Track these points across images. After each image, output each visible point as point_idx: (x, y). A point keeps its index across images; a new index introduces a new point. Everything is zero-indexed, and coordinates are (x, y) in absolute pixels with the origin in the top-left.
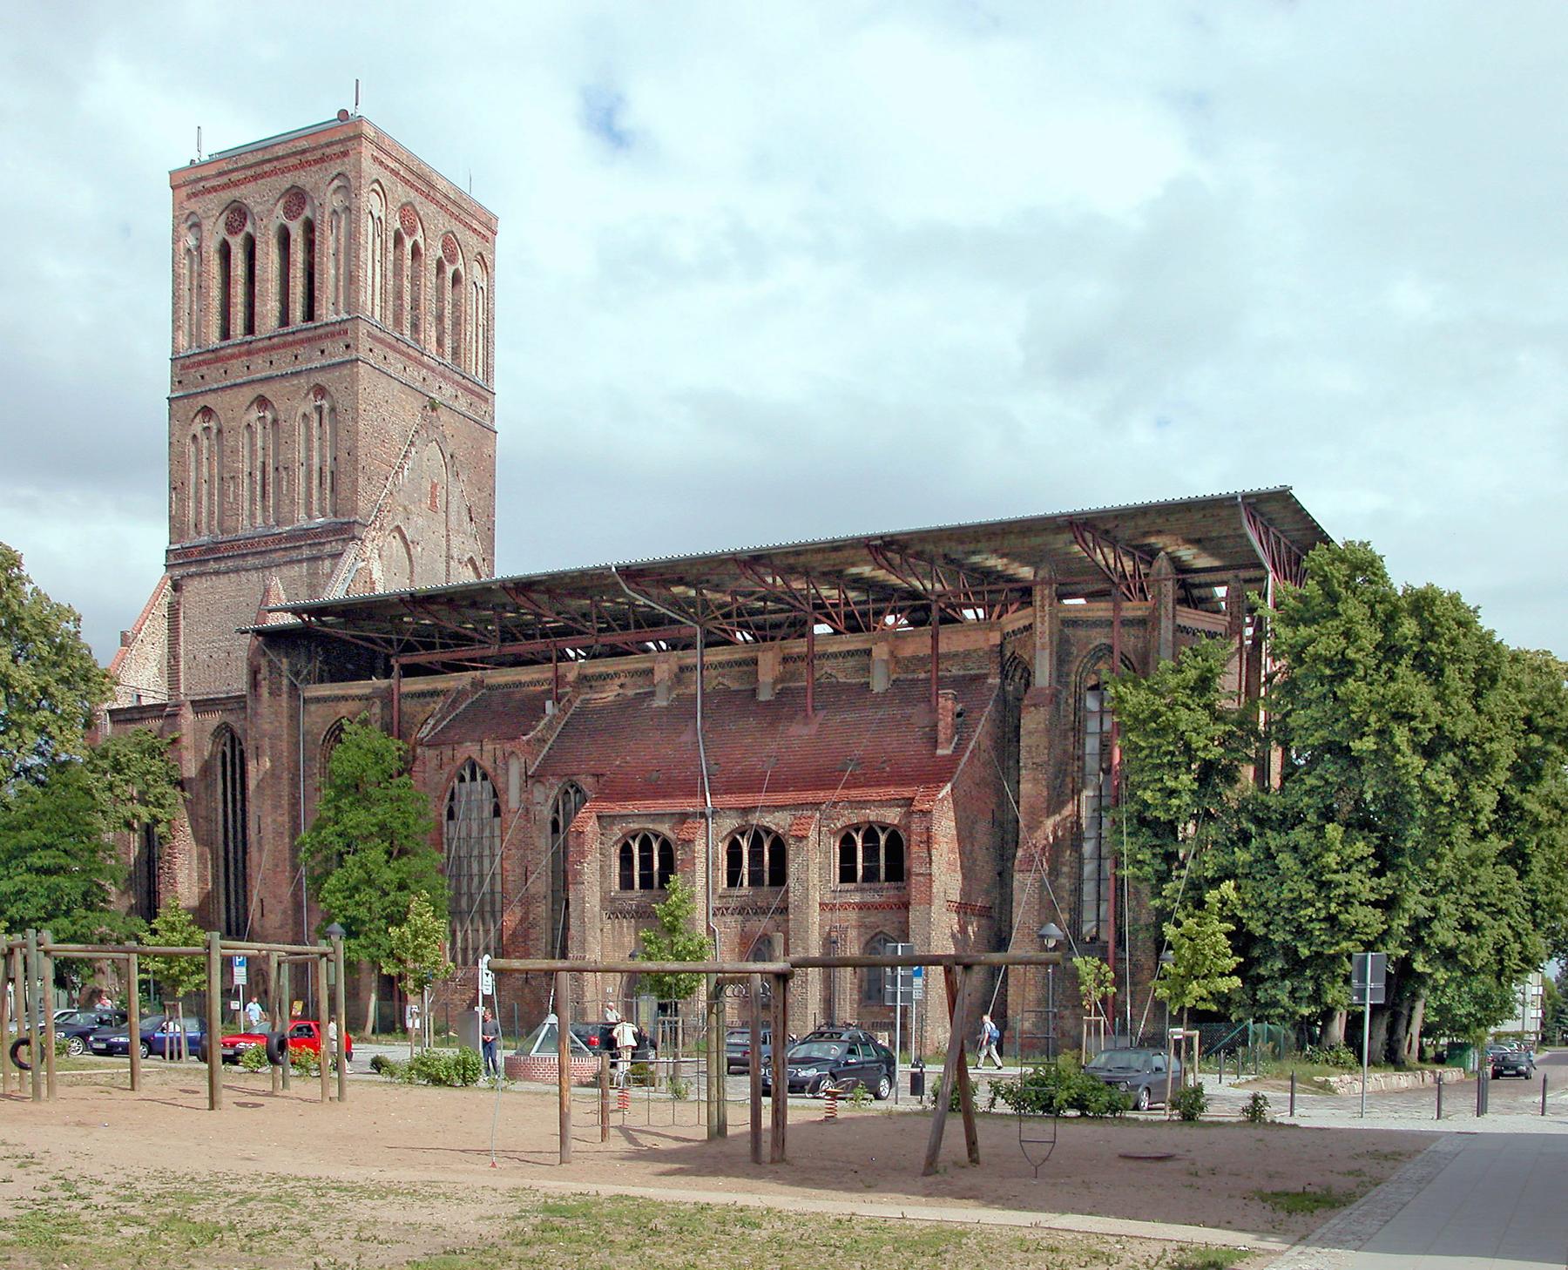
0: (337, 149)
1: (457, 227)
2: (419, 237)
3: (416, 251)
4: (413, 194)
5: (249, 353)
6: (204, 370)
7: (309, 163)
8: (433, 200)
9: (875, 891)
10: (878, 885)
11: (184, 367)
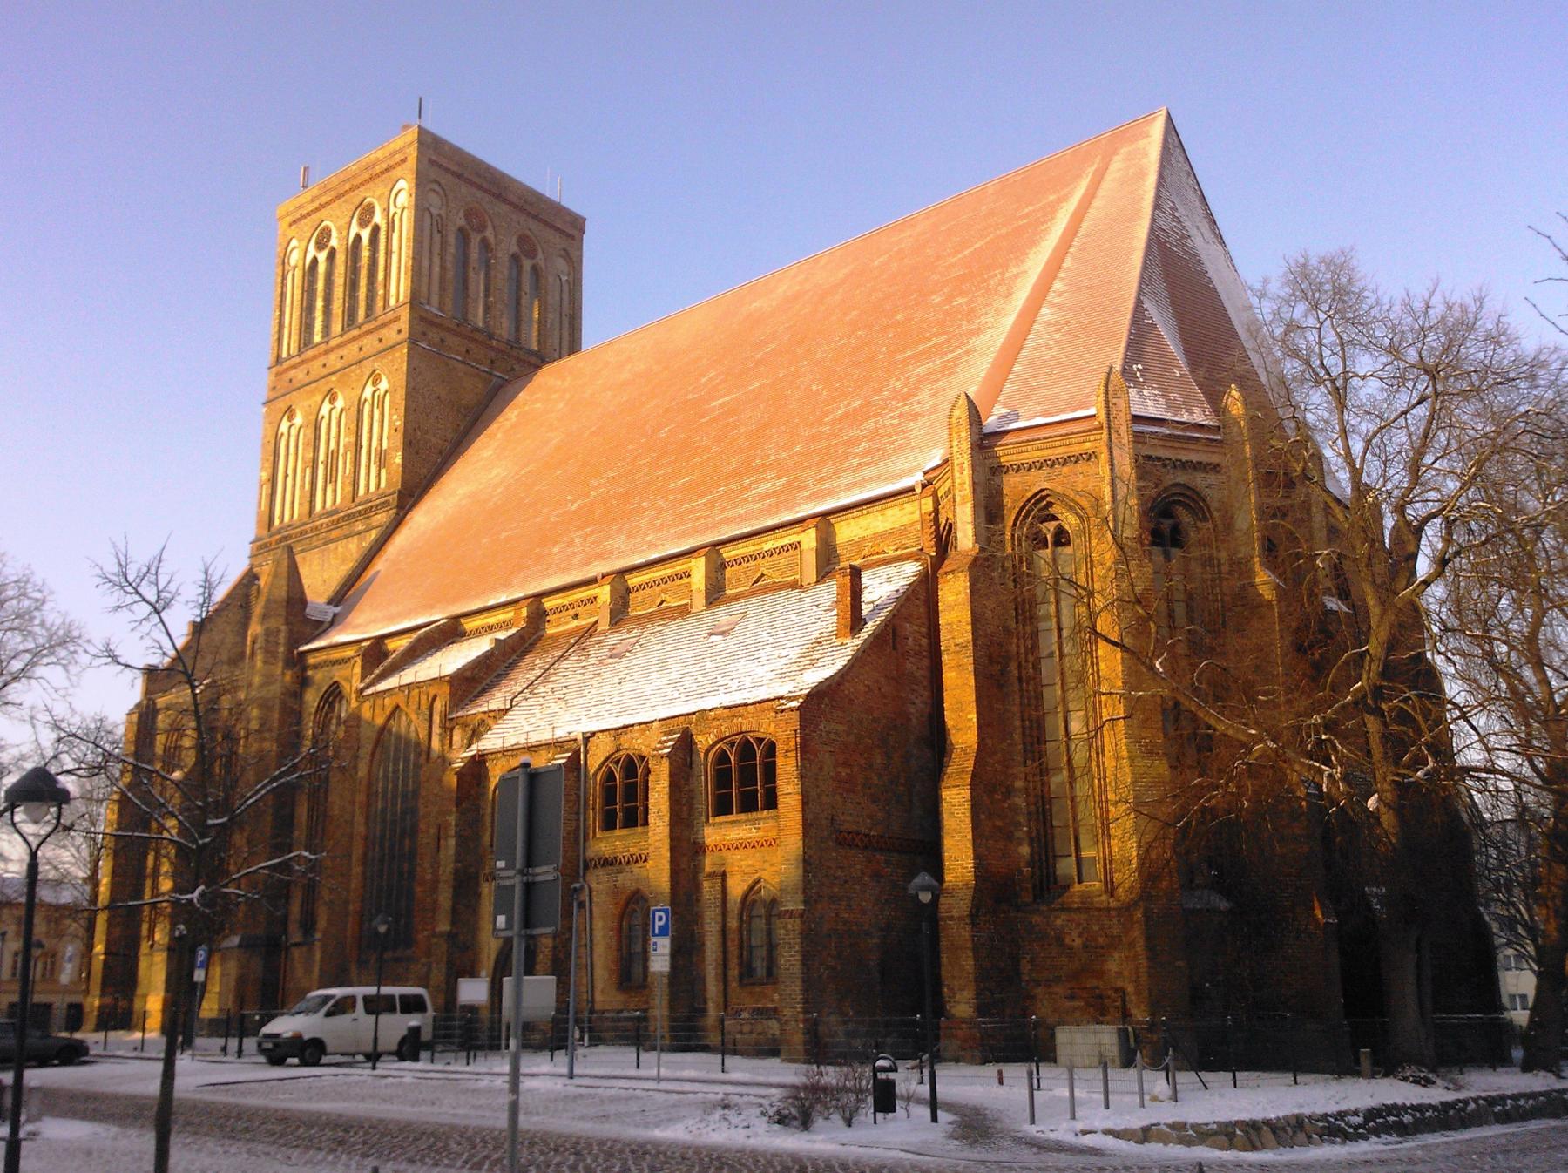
0: (398, 157)
1: (533, 225)
2: (489, 233)
3: (485, 243)
4: (479, 194)
6: (292, 373)
7: (377, 176)
8: (506, 201)
9: (753, 822)
10: (755, 815)
11: (278, 374)
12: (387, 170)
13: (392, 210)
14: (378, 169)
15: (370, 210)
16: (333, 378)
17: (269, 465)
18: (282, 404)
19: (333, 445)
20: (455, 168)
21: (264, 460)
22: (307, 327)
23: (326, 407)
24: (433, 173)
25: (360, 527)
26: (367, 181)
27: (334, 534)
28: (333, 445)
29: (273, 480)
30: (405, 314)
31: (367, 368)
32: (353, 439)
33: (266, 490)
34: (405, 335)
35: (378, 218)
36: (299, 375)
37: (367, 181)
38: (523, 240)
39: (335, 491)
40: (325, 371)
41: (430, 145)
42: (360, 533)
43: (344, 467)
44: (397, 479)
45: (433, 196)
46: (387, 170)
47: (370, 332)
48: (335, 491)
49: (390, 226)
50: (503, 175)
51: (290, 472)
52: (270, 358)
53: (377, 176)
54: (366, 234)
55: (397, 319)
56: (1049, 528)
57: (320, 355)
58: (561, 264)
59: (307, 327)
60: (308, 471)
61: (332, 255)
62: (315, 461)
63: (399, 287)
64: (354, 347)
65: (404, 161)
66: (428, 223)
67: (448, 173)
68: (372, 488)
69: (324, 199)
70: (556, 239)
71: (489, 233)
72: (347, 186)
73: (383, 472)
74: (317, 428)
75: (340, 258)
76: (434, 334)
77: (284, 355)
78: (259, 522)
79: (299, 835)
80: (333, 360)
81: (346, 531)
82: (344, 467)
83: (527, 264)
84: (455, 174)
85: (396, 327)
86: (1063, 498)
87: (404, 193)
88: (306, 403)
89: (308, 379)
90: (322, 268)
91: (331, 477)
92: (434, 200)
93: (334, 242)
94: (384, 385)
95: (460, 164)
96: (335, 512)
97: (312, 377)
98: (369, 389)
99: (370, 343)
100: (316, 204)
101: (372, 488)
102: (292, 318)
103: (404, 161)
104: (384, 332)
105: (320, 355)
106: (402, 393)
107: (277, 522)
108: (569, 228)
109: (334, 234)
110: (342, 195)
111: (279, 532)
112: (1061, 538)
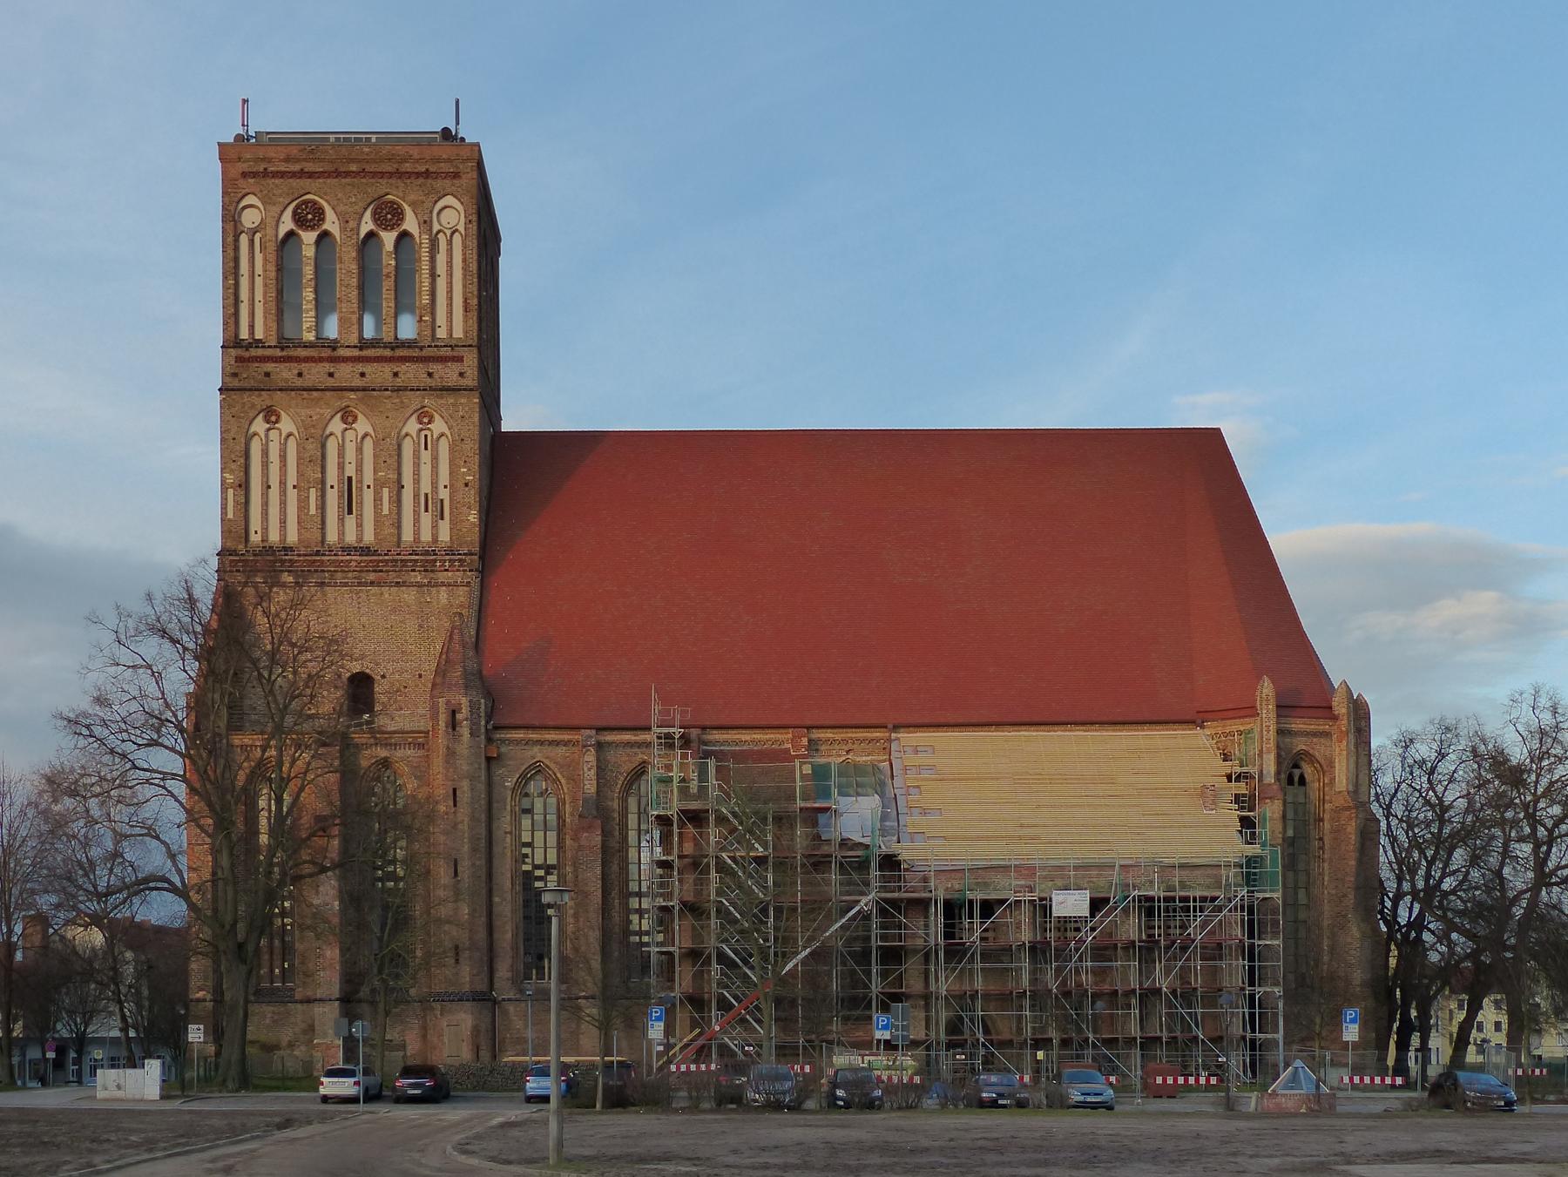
6: (269, 367)
11: (239, 359)
13: (436, 227)
15: (399, 215)
19: (350, 471)
29: (244, 486)
31: (414, 400)
35: (410, 224)
37: (391, 175)
40: (331, 382)
42: (419, 585)
46: (427, 174)
48: (360, 525)
51: (274, 481)
53: (409, 174)
65: (456, 175)
69: (310, 167)
88: (304, 412)
94: (438, 426)
96: (366, 551)
97: (307, 381)
109: (330, 215)
112: (1302, 781)
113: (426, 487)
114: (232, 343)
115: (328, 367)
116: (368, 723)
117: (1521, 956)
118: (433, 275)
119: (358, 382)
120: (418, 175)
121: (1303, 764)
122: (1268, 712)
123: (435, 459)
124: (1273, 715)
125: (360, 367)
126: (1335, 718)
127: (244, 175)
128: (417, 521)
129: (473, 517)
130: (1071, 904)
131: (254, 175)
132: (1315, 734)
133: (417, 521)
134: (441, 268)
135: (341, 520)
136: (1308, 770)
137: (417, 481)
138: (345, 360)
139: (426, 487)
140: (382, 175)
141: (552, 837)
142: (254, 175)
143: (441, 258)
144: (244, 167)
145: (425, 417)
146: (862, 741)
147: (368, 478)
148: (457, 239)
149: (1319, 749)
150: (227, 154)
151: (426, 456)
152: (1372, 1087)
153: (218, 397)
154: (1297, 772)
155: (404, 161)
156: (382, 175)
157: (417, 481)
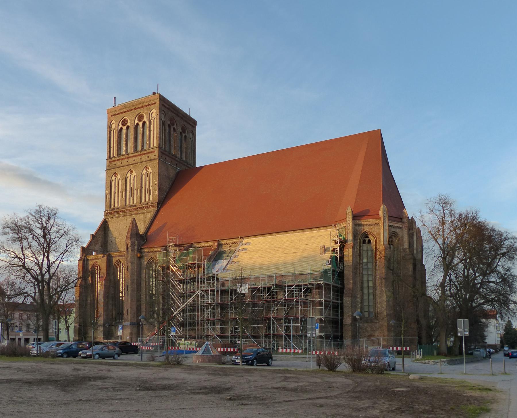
0: (152, 102)
2: (175, 126)
4: (173, 114)
5: (128, 158)
6: (115, 162)
7: (145, 106)
11: (110, 162)
12: (149, 105)
13: (151, 118)
14: (145, 104)
15: (142, 116)
16: (132, 166)
17: (109, 189)
18: (113, 171)
19: (132, 186)
20: (168, 107)
21: (106, 187)
22: (119, 148)
23: (129, 175)
24: (163, 108)
25: (144, 211)
26: (141, 107)
27: (134, 212)
28: (132, 186)
29: (110, 193)
30: (157, 150)
31: (144, 164)
32: (140, 185)
33: (108, 196)
34: (157, 157)
35: (145, 119)
36: (118, 163)
37: (141, 107)
38: (182, 128)
39: (133, 199)
40: (128, 164)
41: (162, 99)
42: (144, 213)
43: (136, 193)
44: (156, 199)
45: (162, 115)
46: (149, 105)
47: (145, 154)
48: (133, 199)
49: (150, 123)
50: (179, 108)
51: (116, 192)
52: (106, 157)
53: (145, 106)
54: (141, 124)
55: (155, 151)
56: (367, 239)
57: (126, 158)
58: (191, 135)
59: (119, 148)
60: (124, 193)
61: (128, 127)
62: (126, 190)
63: (155, 142)
64: (139, 157)
65: (155, 103)
66: (162, 124)
67: (167, 108)
68: (147, 200)
69: (125, 110)
70: (190, 127)
71: (175, 126)
72: (133, 108)
73: (151, 196)
74: (126, 180)
75: (132, 130)
76: (164, 157)
77: (112, 156)
78: (106, 206)
79: (122, 302)
80: (131, 161)
81: (139, 212)
82: (136, 193)
83: (184, 135)
84: (168, 108)
85: (154, 154)
86: (371, 233)
87: (155, 113)
88: (122, 172)
89: (121, 165)
90: (124, 131)
91: (131, 195)
92: (163, 116)
93: (129, 124)
94: (150, 170)
95: (169, 105)
96: (134, 206)
97: (123, 165)
98: (144, 171)
99: (145, 157)
100: (121, 111)
101: (147, 200)
102: (114, 145)
103: (155, 103)
104: (149, 155)
105: (126, 158)
106: (156, 175)
107: (112, 206)
108: (193, 123)
109: (129, 121)
110: (132, 110)
111: (114, 209)
112: (369, 242)
113: (147, 187)
114: (109, 157)
115: (127, 160)
116: (399, 263)
117: (516, 303)
118: (150, 131)
119: (133, 162)
120: (147, 106)
121: (393, 237)
122: (349, 218)
123: (150, 179)
124: (351, 219)
125: (134, 158)
126: (380, 218)
127: (112, 116)
128: (145, 196)
129: (157, 193)
130: (245, 289)
131: (113, 115)
132: (372, 225)
133: (145, 196)
134: (152, 129)
135: (130, 199)
136: (371, 238)
137: (146, 186)
138: (130, 157)
139: (147, 187)
140: (139, 108)
141: (365, 285)
142: (113, 115)
143: (152, 126)
144: (112, 114)
145: (147, 168)
146: (233, 243)
147: (135, 188)
148: (155, 119)
149: (373, 230)
150: (109, 111)
151: (147, 179)
152: (286, 353)
153: (105, 172)
154: (367, 239)
155: (143, 103)
156: (139, 108)
157: (146, 186)
